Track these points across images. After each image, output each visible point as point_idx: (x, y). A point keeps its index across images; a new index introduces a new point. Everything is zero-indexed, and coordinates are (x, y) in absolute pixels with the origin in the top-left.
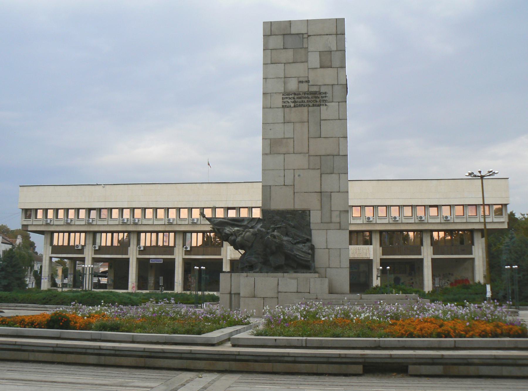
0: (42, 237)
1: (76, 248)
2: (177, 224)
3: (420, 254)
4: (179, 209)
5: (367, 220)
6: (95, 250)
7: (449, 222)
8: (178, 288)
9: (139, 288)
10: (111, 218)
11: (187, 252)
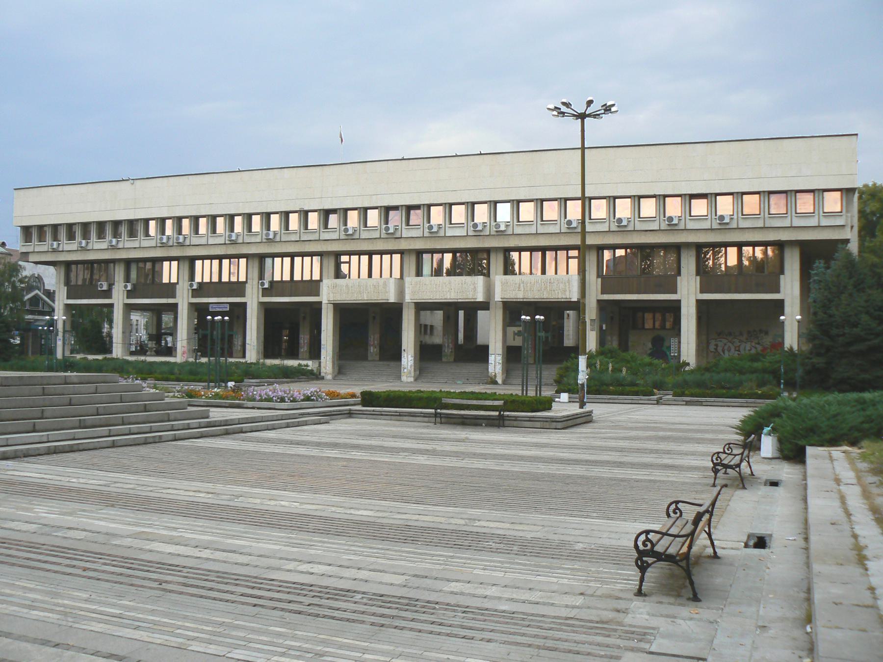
0: (51, 269)
1: (99, 289)
2: (243, 243)
4: (516, 204)
5: (718, 222)
6: (264, 289)
7: (728, 227)
8: (252, 355)
10: (451, 224)
11: (266, 292)
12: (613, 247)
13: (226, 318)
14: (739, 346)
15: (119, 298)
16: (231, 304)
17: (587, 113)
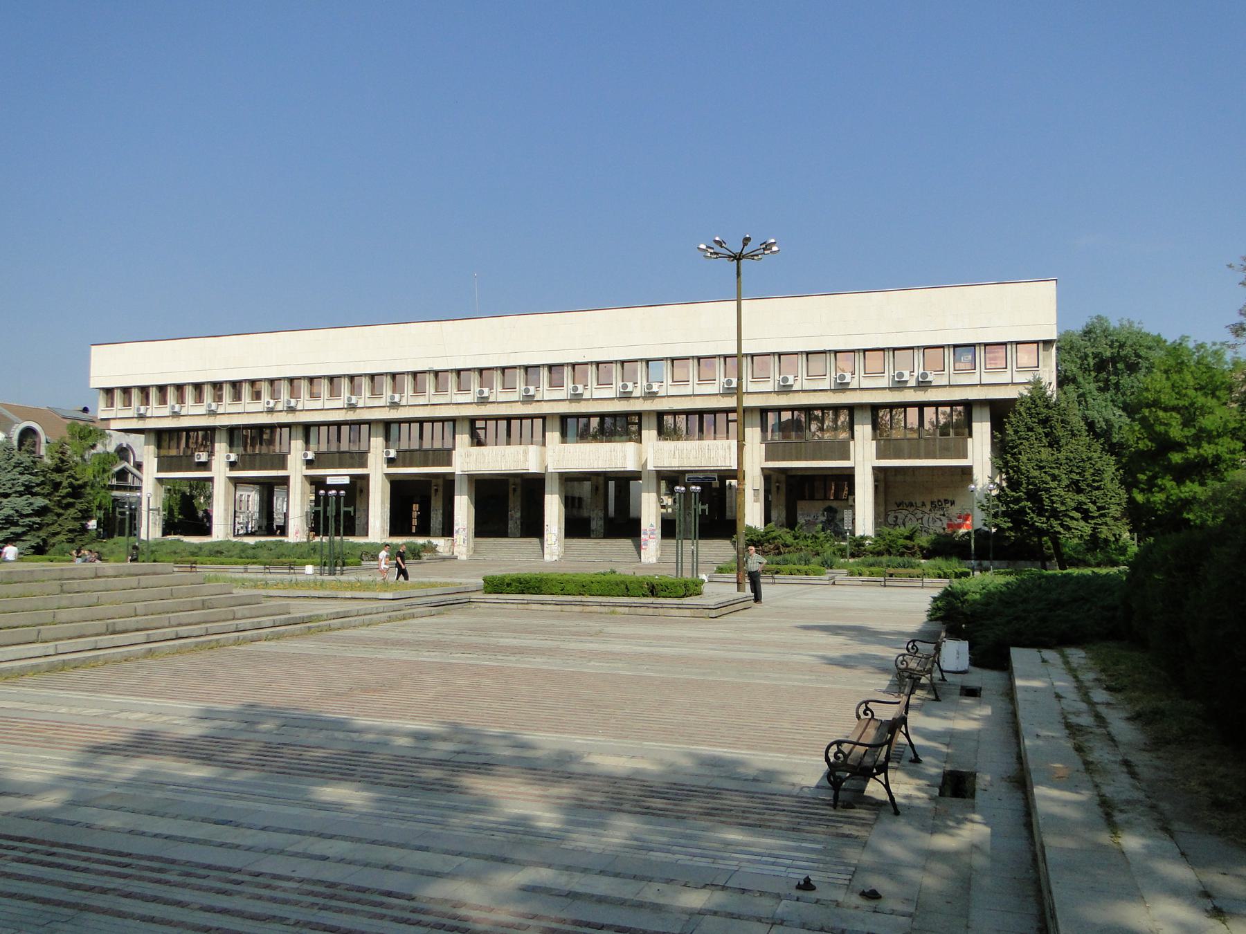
1: (196, 460)
9: (394, 532)
12: (779, 410)
13: (342, 492)
14: (922, 518)
15: (220, 471)
16: (351, 476)
17: (744, 253)
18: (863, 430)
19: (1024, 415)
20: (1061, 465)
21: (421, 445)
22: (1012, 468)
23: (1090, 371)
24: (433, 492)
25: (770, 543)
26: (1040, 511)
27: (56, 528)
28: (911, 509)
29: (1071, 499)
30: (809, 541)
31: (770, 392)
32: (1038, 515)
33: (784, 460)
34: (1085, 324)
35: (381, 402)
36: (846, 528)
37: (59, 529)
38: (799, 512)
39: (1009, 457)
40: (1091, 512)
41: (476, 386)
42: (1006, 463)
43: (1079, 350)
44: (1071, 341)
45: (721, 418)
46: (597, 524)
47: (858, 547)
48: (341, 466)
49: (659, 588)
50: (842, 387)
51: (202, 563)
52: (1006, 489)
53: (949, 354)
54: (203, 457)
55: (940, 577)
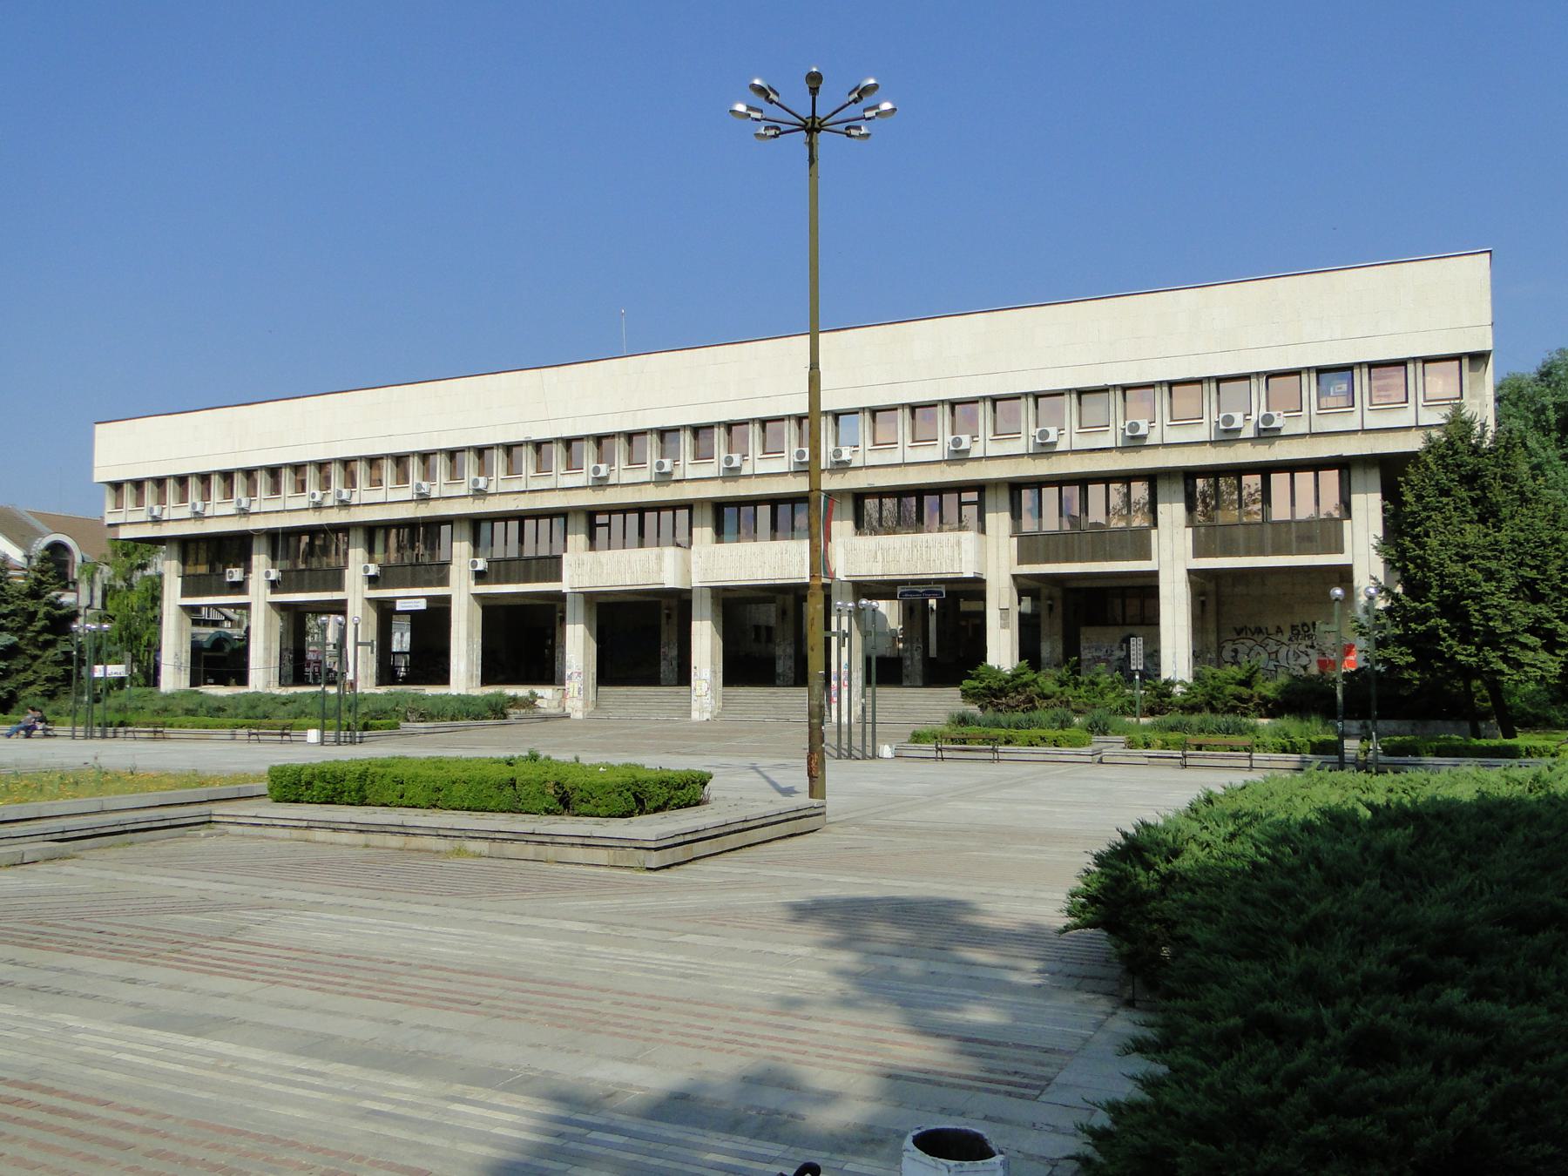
1: (228, 580)
3: (1147, 556)
14: (1277, 652)
16: (429, 598)
18: (1172, 512)
19: (1434, 468)
20: (1502, 552)
21: (521, 551)
22: (1412, 560)
23: (1551, 430)
24: (664, 621)
25: (1019, 693)
26: (1465, 636)
27: (30, 676)
28: (1259, 638)
29: (1523, 611)
30: (1083, 689)
31: (1022, 455)
32: (1461, 642)
33: (1047, 561)
34: (1540, 364)
35: (463, 490)
36: (1133, 668)
37: (32, 678)
38: (1083, 644)
39: (1407, 541)
40: (1561, 636)
41: (590, 461)
42: (1402, 554)
43: (1532, 400)
44: (1519, 387)
45: (950, 500)
46: (914, 663)
47: (1160, 700)
48: (414, 585)
49: (576, 796)
50: (1135, 443)
51: (180, 727)
52: (1404, 597)
53: (1309, 383)
54: (236, 574)
55: (1284, 751)
